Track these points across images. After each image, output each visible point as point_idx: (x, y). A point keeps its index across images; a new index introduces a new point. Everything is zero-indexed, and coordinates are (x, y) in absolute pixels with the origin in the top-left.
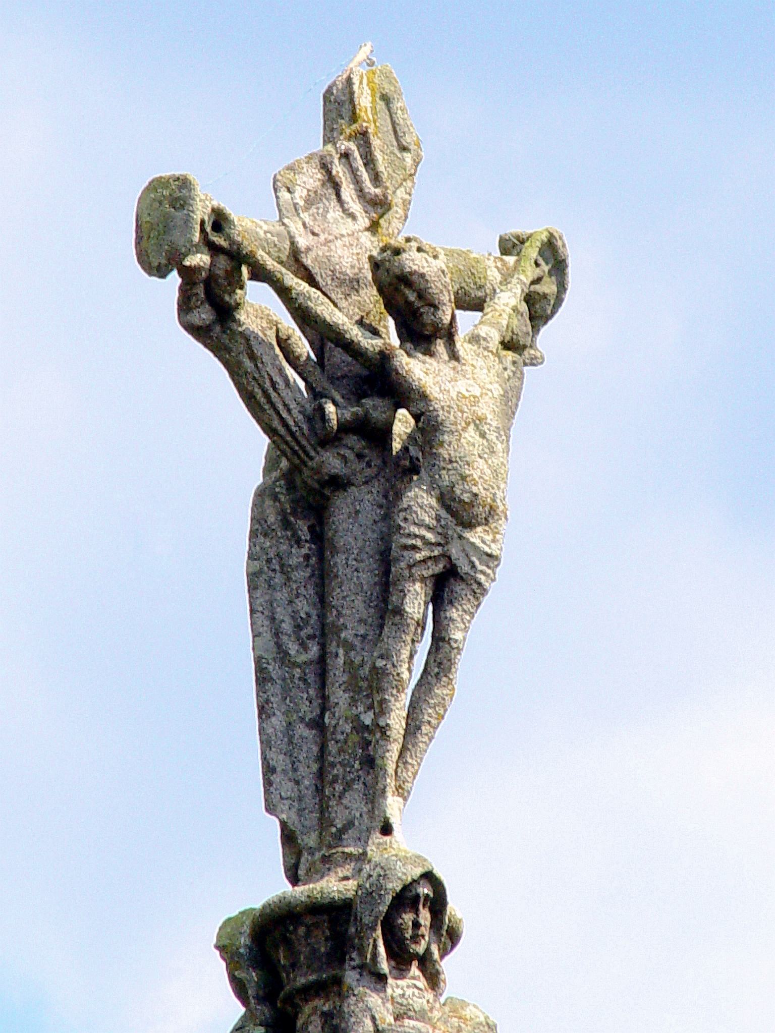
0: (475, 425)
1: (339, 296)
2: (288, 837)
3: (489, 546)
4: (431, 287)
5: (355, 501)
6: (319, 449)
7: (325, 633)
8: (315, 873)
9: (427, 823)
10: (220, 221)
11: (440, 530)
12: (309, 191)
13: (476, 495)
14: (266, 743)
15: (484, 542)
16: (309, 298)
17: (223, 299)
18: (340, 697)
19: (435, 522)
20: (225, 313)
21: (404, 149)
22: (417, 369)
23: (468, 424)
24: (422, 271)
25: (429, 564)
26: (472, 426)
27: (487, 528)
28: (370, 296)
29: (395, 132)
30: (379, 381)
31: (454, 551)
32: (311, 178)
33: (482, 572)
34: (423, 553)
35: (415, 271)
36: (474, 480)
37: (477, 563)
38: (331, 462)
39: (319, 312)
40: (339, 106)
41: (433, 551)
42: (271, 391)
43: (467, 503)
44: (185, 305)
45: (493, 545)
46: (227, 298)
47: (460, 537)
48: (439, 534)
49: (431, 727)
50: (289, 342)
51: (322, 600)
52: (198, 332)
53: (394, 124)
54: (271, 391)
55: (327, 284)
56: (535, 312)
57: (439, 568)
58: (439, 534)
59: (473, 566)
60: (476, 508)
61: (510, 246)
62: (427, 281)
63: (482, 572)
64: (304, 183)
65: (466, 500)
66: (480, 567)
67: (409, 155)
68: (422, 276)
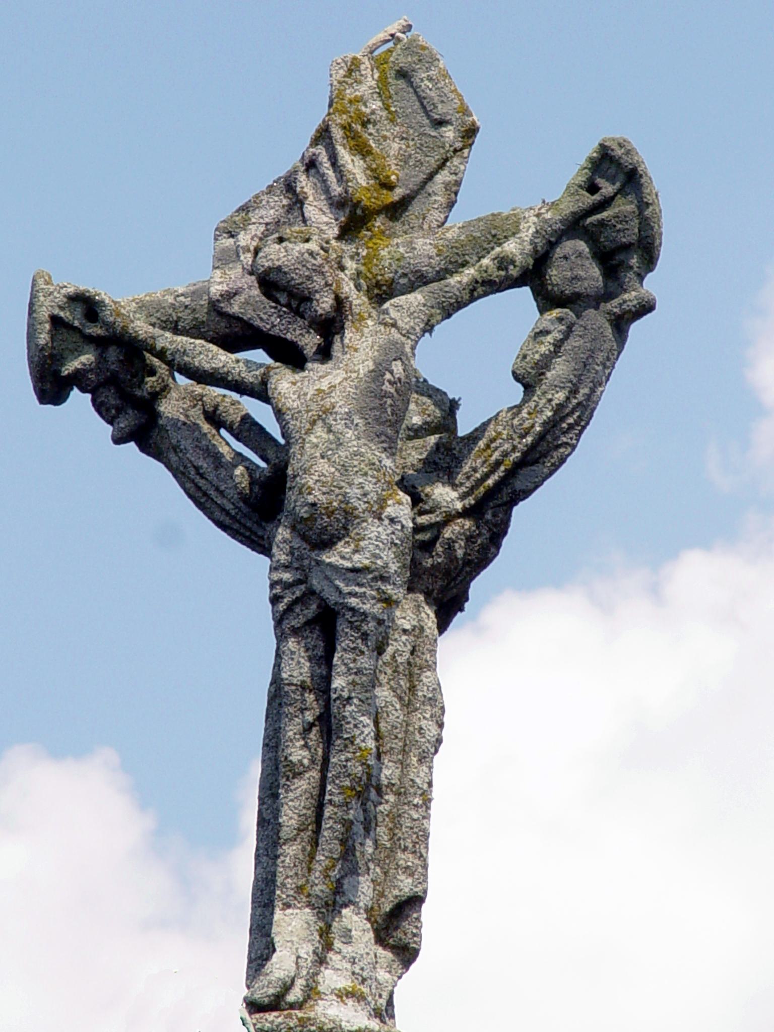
0: (323, 420)
1: (298, 332)
3: (350, 559)
4: (293, 279)
6: (264, 524)
11: (296, 565)
12: (267, 224)
13: (314, 505)
15: (343, 558)
16: (185, 353)
17: (135, 396)
19: (289, 558)
21: (440, 123)
23: (313, 423)
24: (277, 263)
25: (297, 610)
26: (320, 423)
27: (347, 539)
29: (423, 107)
31: (316, 582)
33: (350, 594)
34: (286, 600)
35: (270, 268)
36: (309, 487)
37: (341, 585)
39: (197, 364)
41: (293, 593)
42: (198, 479)
43: (306, 519)
45: (356, 557)
46: (138, 393)
47: (318, 563)
48: (297, 569)
49: (334, 806)
50: (218, 412)
53: (420, 99)
54: (198, 479)
55: (274, 326)
56: (604, 247)
57: (313, 609)
58: (297, 569)
59: (339, 591)
60: (319, 521)
62: (285, 273)
63: (355, 595)
64: (262, 217)
65: (305, 516)
66: (346, 590)
67: (450, 127)
68: (279, 269)
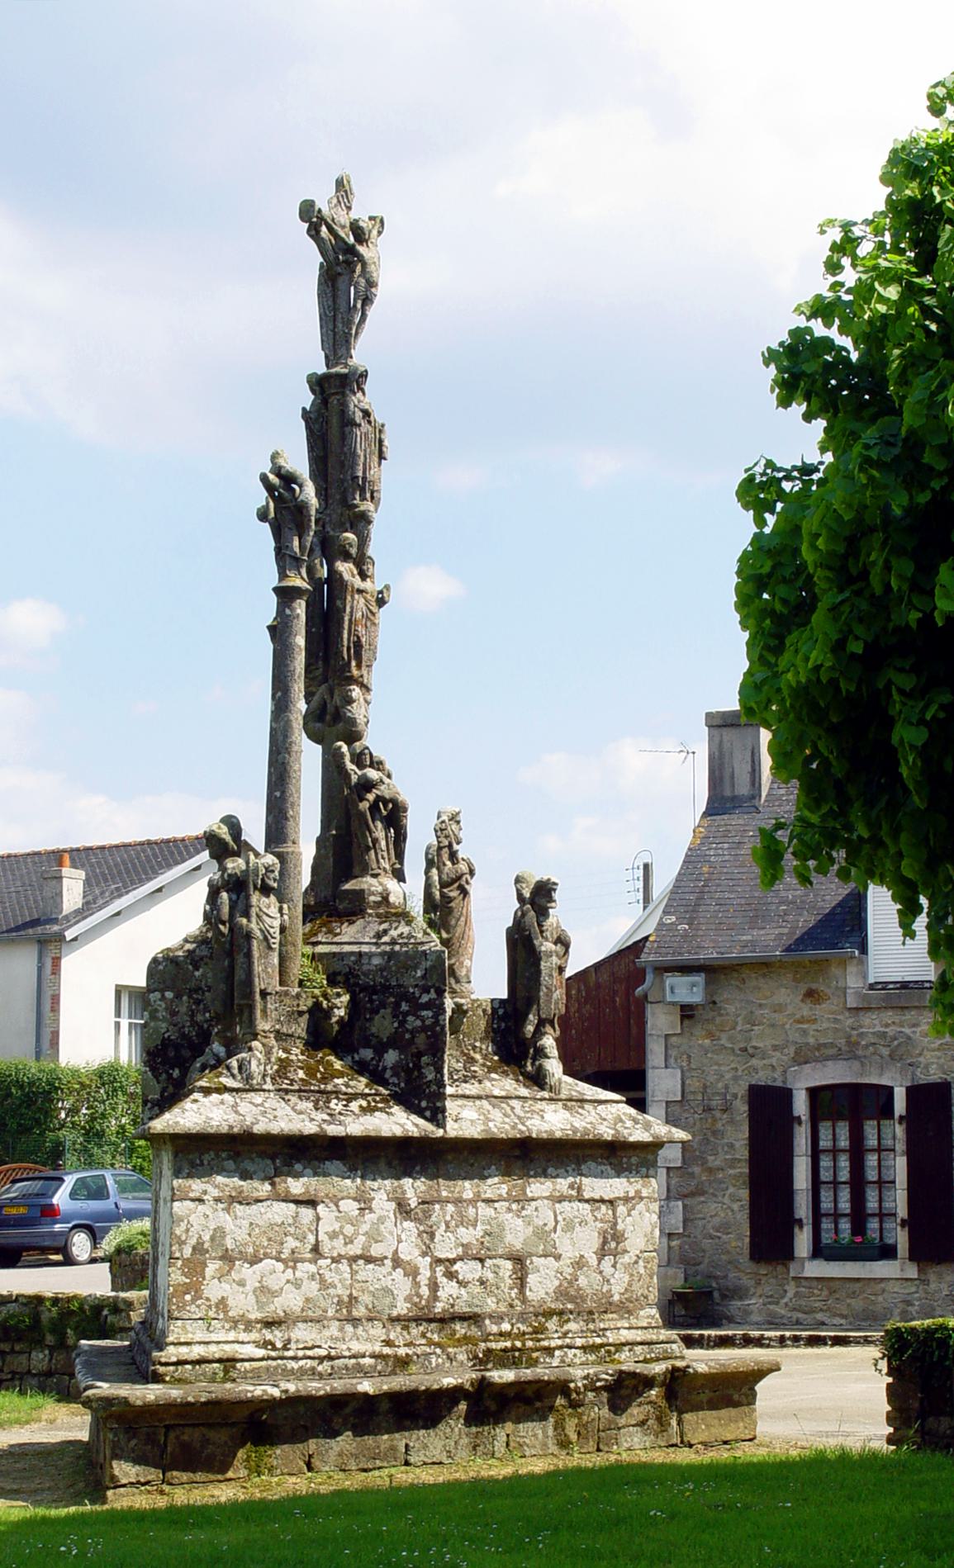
2: (327, 357)
5: (343, 273)
7: (335, 310)
8: (334, 366)
9: (361, 355)
10: (320, 211)
14: (57, 1021)
18: (340, 325)
20: (318, 232)
22: (361, 249)
28: (347, 229)
30: (351, 250)
32: (335, 201)
38: (339, 269)
40: (340, 184)
44: (308, 231)
51: (334, 302)
52: (311, 236)
53: (641, 1343)
61: (371, 218)
